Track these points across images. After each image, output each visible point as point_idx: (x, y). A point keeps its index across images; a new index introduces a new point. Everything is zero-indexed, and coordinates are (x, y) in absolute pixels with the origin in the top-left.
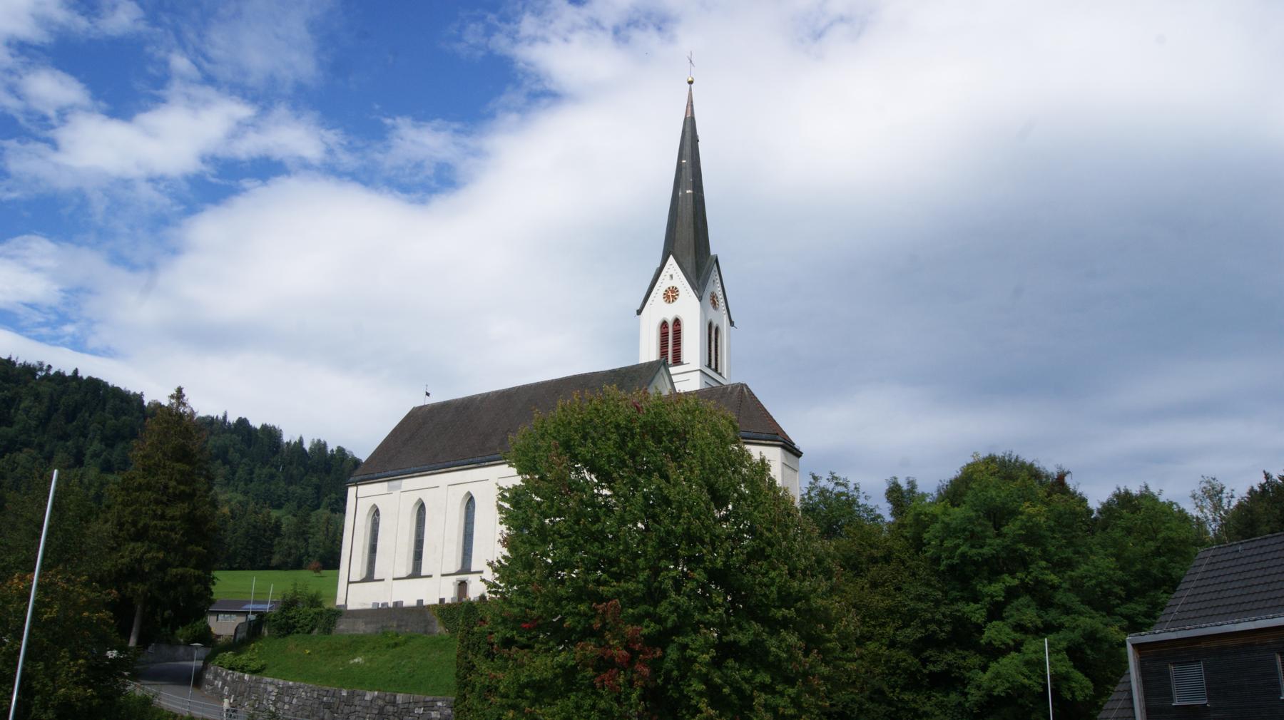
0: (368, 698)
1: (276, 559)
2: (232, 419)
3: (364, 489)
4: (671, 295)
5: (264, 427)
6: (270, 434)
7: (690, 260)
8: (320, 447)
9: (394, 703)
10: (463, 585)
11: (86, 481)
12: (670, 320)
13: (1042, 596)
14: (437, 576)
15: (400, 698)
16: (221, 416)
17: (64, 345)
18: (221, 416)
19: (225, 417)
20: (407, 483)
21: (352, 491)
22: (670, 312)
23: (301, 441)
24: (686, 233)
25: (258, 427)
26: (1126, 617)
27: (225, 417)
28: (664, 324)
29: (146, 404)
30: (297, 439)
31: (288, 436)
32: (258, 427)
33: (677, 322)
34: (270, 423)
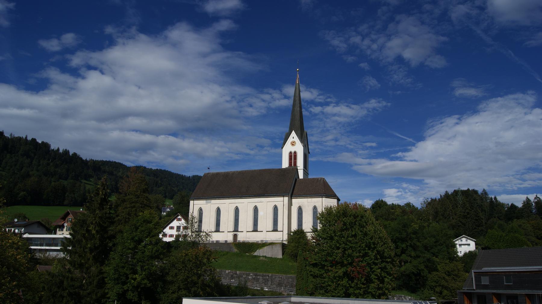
0: (227, 272)
1: (66, 202)
2: (29, 138)
3: (196, 202)
4: (293, 144)
5: (43, 142)
6: (45, 146)
7: (299, 132)
8: (66, 152)
9: (236, 274)
10: (235, 236)
11: (297, 245)
12: (293, 151)
13: (414, 248)
14: (226, 232)
15: (238, 272)
16: (24, 137)
17: (314, 223)
18: (24, 137)
19: (26, 137)
20: (213, 201)
21: (191, 202)
22: (293, 149)
23: (58, 149)
24: (298, 123)
25: (40, 142)
26: (432, 253)
27: (26, 137)
28: (291, 153)
29: (71, 154)
30: (56, 148)
31: (53, 147)
32: (40, 142)
33: (295, 152)
34: (45, 141)
